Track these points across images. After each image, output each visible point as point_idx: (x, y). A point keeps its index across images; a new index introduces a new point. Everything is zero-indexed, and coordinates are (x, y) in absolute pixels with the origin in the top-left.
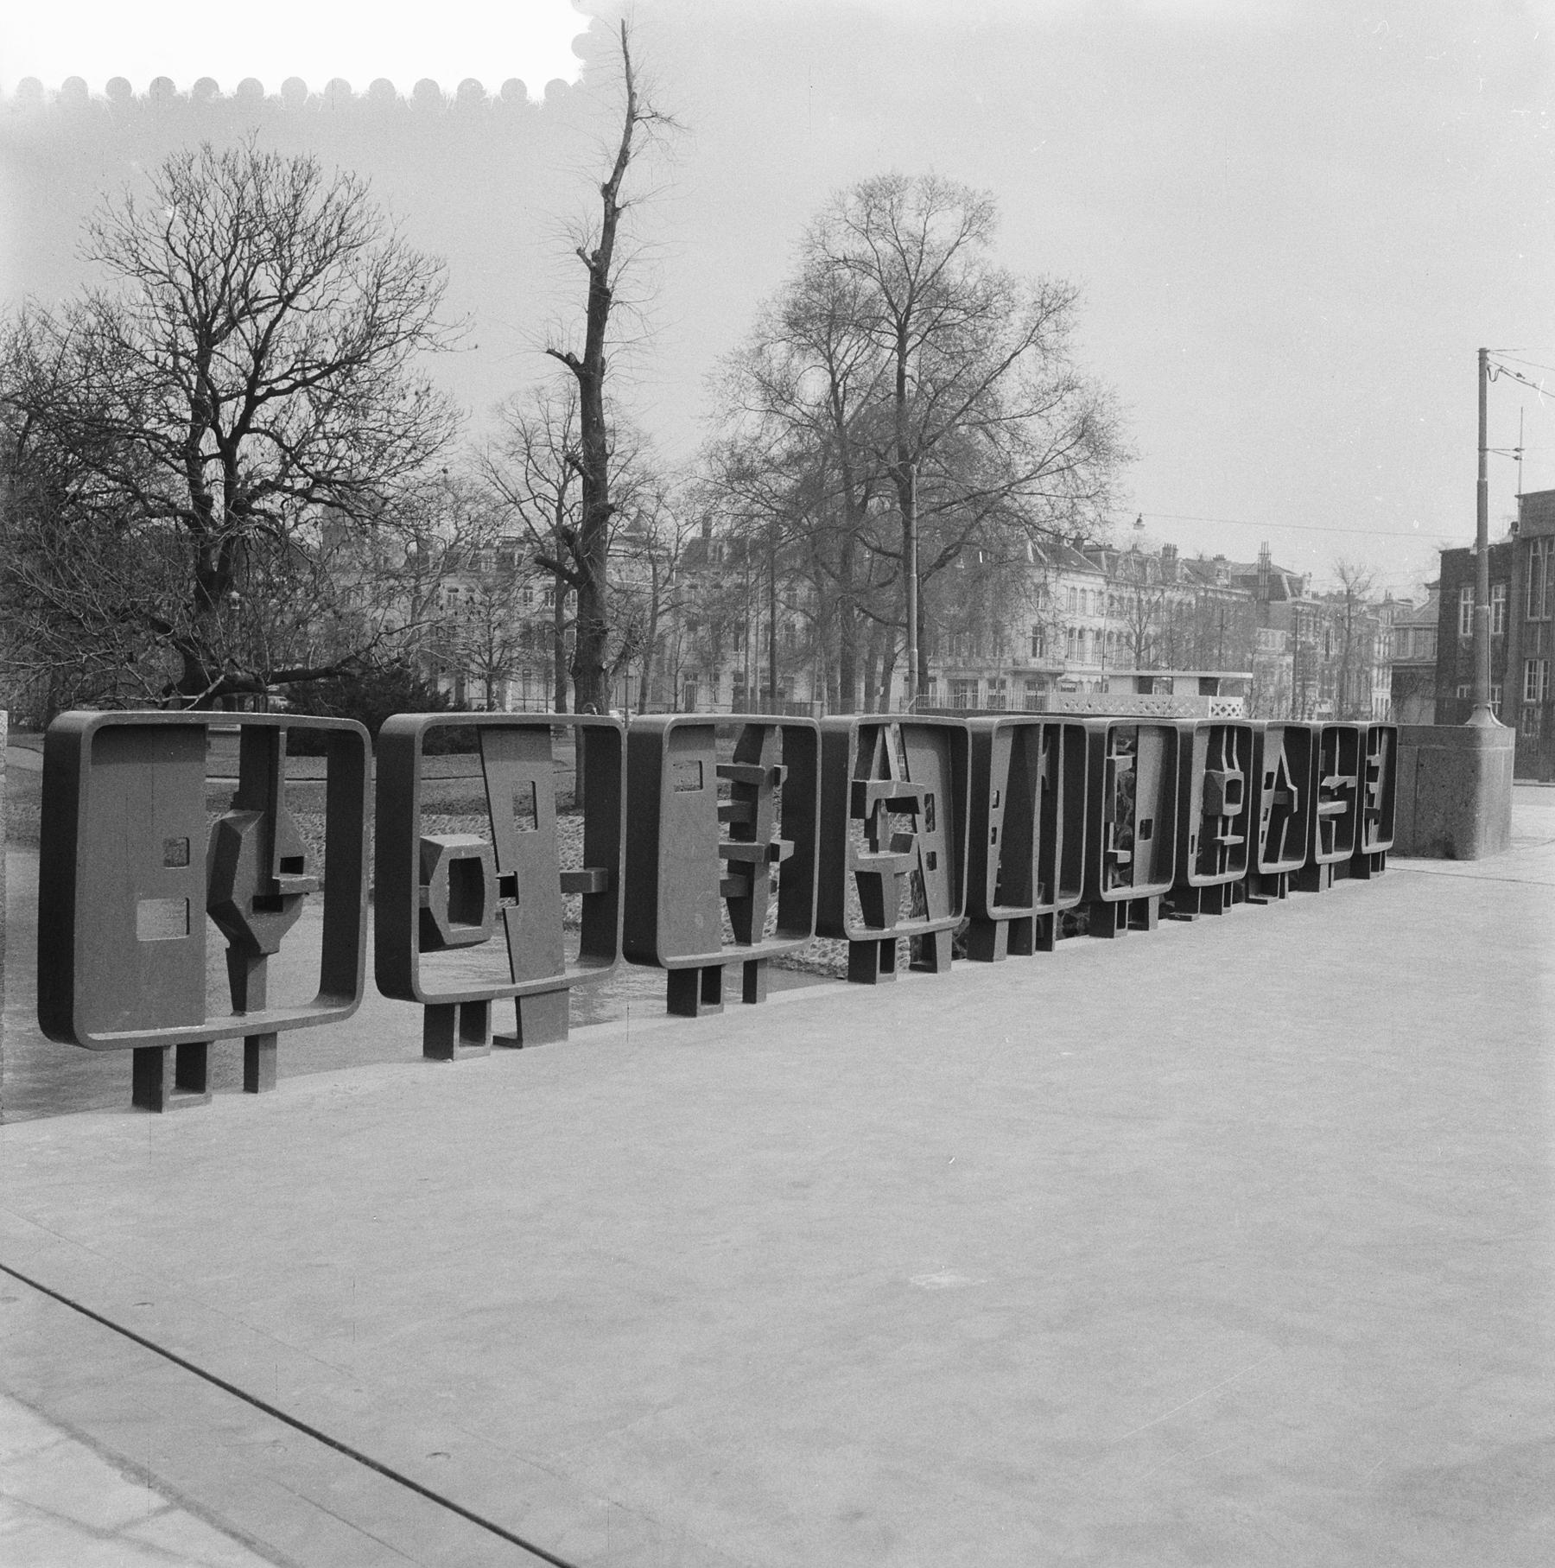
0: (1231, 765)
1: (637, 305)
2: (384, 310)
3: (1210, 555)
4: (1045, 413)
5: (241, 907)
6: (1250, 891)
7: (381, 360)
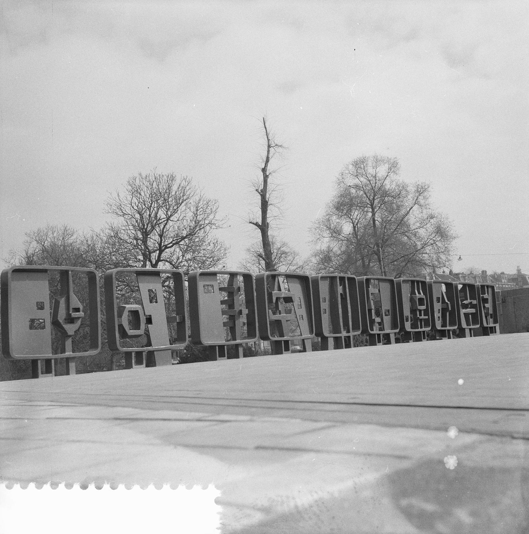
0: (419, 293)
1: (276, 204)
2: (200, 218)
3: (499, 272)
4: (425, 227)
5: (61, 321)
6: (437, 336)
7: (201, 234)
